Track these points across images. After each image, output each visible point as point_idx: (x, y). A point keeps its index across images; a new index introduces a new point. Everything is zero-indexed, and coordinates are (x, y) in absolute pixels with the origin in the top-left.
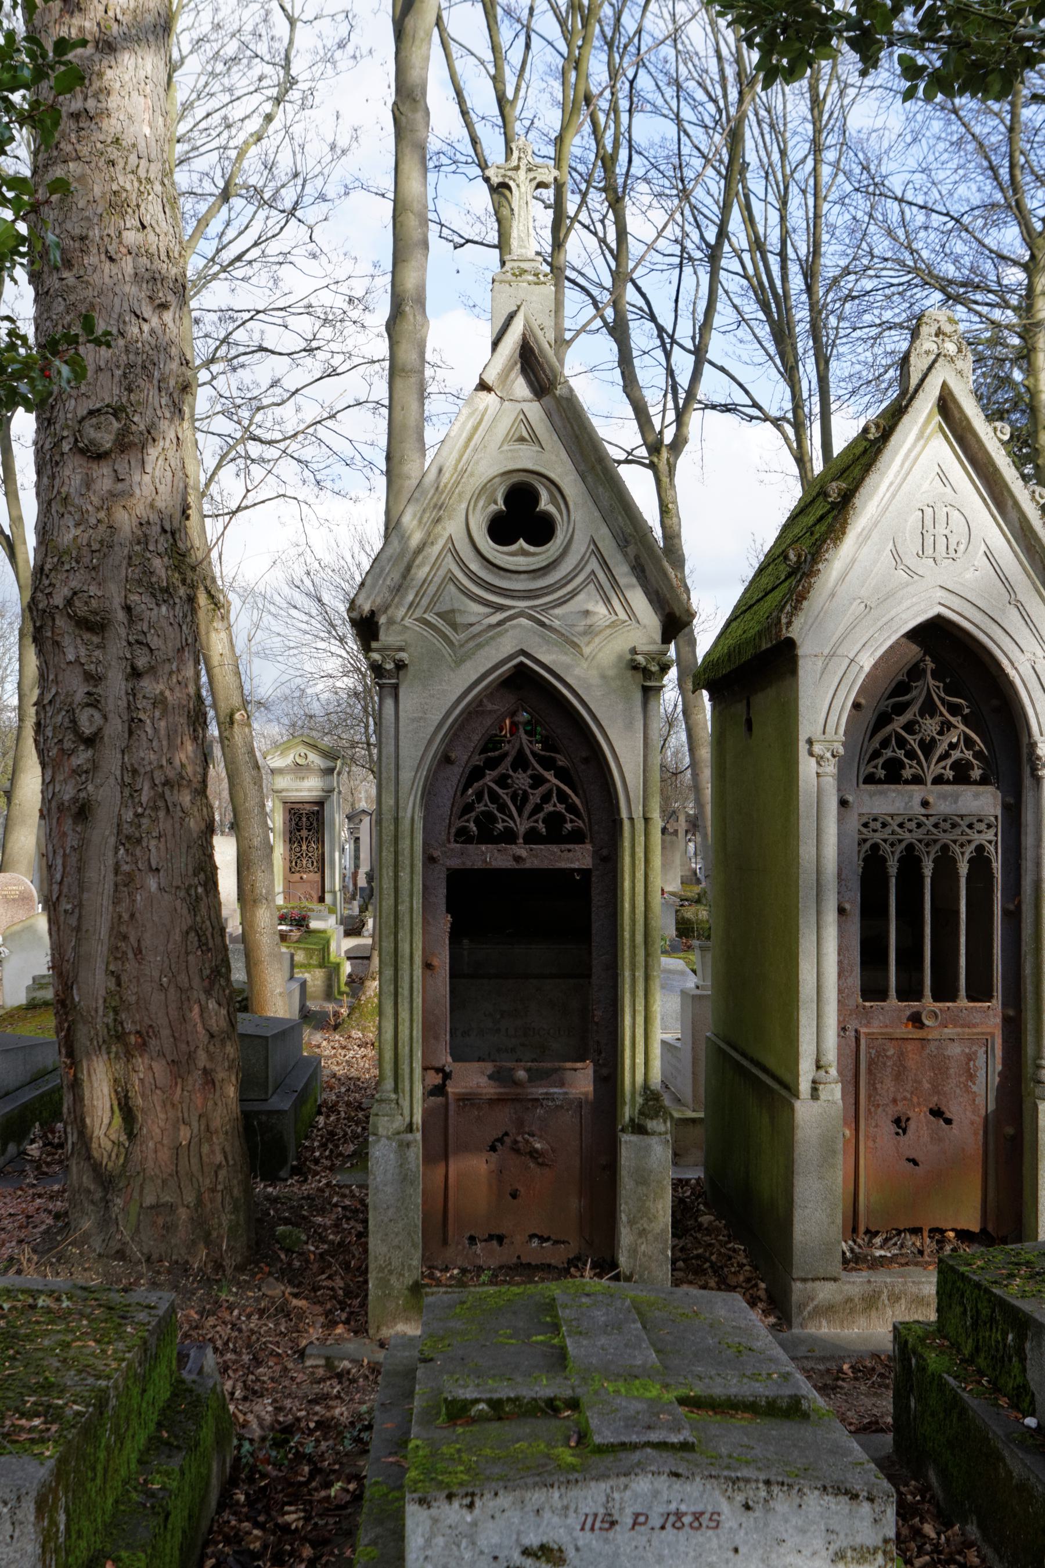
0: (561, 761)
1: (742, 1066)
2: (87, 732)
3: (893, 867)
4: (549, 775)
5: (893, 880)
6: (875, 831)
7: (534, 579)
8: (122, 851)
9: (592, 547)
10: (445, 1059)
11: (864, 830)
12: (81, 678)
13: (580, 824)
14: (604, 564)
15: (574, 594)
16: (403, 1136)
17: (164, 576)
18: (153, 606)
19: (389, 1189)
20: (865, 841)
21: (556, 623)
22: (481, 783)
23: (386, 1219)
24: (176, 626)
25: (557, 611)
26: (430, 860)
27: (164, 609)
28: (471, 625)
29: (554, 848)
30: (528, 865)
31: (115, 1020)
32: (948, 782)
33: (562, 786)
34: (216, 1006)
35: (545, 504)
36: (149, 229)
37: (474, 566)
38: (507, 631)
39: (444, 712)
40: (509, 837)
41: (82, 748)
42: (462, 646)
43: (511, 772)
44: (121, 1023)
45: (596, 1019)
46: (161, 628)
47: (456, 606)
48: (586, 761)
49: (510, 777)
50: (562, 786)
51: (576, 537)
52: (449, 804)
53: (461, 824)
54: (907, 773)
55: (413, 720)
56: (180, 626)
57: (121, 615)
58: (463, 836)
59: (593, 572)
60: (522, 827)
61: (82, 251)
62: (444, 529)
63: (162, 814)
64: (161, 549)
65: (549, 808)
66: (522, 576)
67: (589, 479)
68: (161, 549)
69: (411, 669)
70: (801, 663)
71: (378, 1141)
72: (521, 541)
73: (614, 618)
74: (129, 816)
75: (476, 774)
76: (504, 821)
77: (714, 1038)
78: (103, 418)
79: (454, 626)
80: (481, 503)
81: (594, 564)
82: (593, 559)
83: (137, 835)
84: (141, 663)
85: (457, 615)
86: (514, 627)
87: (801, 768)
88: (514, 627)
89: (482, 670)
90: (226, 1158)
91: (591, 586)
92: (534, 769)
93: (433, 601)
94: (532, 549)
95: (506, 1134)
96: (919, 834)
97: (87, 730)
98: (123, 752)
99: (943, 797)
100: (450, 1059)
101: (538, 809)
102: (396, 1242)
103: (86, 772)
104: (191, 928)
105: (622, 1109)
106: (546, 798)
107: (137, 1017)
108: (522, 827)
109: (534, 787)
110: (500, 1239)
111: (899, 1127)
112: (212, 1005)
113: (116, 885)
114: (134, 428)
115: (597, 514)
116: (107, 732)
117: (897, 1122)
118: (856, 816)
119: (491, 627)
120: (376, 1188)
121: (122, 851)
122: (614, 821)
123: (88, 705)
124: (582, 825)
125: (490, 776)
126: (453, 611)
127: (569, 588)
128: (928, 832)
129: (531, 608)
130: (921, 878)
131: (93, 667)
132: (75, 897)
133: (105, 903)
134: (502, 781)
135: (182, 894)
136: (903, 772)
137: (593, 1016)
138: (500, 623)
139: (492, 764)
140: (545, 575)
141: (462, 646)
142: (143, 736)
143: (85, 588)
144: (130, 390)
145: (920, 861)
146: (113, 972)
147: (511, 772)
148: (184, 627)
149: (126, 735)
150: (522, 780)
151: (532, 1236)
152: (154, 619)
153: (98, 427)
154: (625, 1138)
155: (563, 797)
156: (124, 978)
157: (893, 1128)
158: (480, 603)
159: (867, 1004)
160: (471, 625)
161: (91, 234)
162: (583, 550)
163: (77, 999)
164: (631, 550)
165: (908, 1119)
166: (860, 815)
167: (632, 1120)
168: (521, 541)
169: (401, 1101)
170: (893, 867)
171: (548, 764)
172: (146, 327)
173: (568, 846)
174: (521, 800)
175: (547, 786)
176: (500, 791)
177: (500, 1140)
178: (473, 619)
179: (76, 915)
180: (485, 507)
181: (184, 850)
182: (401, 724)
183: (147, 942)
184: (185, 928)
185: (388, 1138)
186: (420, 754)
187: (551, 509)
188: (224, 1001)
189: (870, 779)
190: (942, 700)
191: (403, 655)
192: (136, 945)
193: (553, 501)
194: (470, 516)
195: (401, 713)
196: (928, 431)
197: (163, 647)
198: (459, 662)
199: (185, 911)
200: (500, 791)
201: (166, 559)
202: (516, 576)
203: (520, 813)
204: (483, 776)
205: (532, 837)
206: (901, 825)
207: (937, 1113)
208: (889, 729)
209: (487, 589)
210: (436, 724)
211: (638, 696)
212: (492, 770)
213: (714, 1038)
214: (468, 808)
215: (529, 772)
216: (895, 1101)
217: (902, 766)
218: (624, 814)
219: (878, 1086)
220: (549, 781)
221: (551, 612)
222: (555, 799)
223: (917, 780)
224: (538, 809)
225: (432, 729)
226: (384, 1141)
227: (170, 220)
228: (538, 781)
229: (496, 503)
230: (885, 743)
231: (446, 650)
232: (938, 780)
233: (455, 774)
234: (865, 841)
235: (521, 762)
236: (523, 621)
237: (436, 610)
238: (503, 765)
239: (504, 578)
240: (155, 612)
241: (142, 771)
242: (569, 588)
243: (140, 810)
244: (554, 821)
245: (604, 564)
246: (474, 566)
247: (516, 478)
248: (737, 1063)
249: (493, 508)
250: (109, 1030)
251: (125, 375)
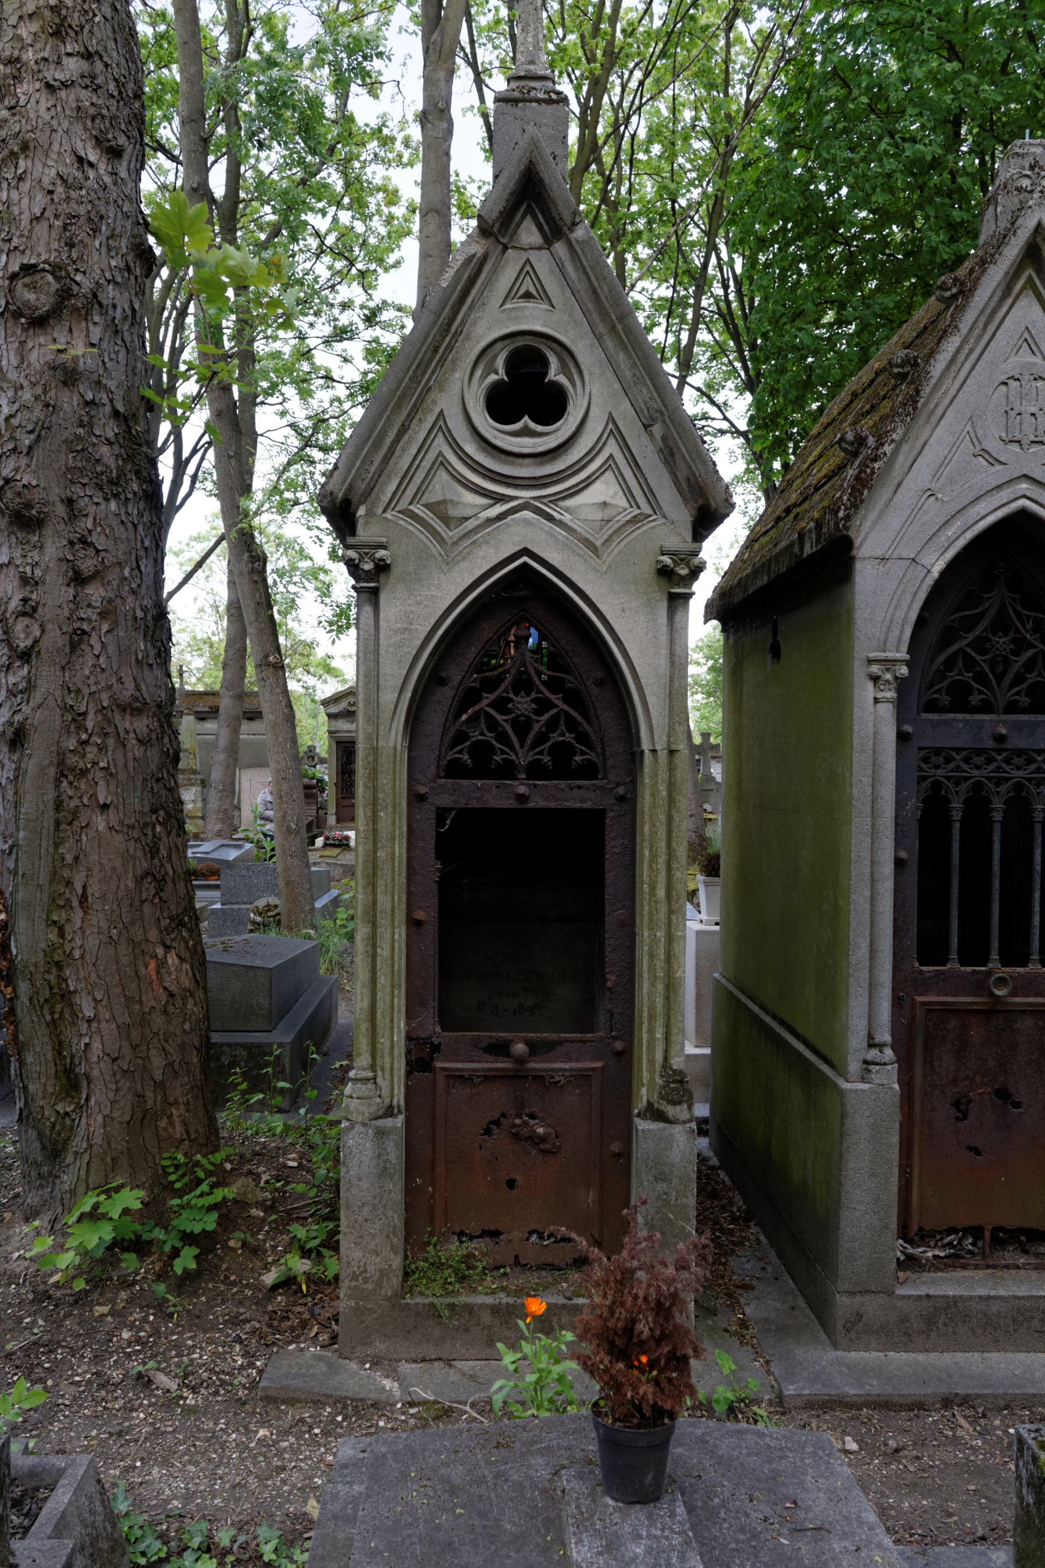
0: (571, 683)
1: (762, 1021)
2: (22, 645)
3: (998, 807)
4: (555, 699)
5: (997, 828)
6: (937, 767)
7: (542, 464)
8: (65, 784)
9: (610, 426)
10: (431, 1027)
11: (925, 766)
12: (16, 582)
13: (592, 756)
14: (624, 446)
15: (588, 483)
16: (380, 1123)
17: (113, 466)
18: (99, 500)
19: (365, 1184)
20: (925, 778)
21: (567, 518)
22: (477, 707)
23: (360, 1219)
24: (129, 526)
25: (569, 503)
26: (416, 799)
27: (113, 505)
28: (466, 519)
29: (563, 784)
30: (531, 805)
31: (59, 976)
32: (1024, 711)
33: (571, 711)
34: (177, 961)
35: (554, 374)
36: (96, 58)
37: (470, 448)
38: (508, 526)
39: (433, 621)
40: (507, 771)
41: (18, 663)
42: (455, 543)
43: (512, 696)
44: (66, 980)
45: (609, 984)
46: (110, 526)
47: (449, 496)
48: (600, 683)
49: (511, 700)
50: (571, 711)
51: (591, 414)
52: (440, 731)
53: (451, 755)
54: (975, 699)
55: (396, 631)
56: (135, 526)
57: (61, 510)
58: (454, 770)
59: (611, 456)
60: (523, 757)
61: (14, 77)
62: (434, 402)
63: (111, 742)
64: (110, 434)
65: (556, 737)
66: (527, 461)
67: (609, 343)
68: (110, 434)
69: (395, 571)
70: (858, 565)
71: (351, 1128)
72: (526, 418)
73: (638, 511)
74: (72, 743)
75: (470, 697)
76: (503, 752)
77: (724, 981)
78: (38, 276)
79: (446, 520)
80: (479, 373)
81: (612, 448)
82: (612, 441)
83: (81, 765)
84: (87, 565)
85: (449, 506)
86: (517, 522)
87: (856, 691)
88: (517, 522)
89: (478, 573)
90: (187, 1131)
91: (609, 475)
92: (539, 691)
93: (419, 492)
94: (539, 428)
95: (504, 1115)
96: (988, 770)
97: (23, 644)
98: (63, 668)
99: (1018, 727)
100: (438, 1029)
101: (542, 738)
102: (372, 1246)
103: (21, 692)
104: (146, 874)
105: (639, 1091)
106: (552, 725)
107: (82, 975)
108: (523, 757)
109: (539, 712)
110: (495, 1234)
111: (959, 1111)
112: (172, 960)
113: (58, 823)
114: (75, 288)
115: (617, 386)
116: (45, 643)
117: (957, 1105)
118: (916, 750)
119: (490, 521)
120: (349, 1182)
121: (65, 784)
122: (633, 754)
123: (24, 614)
124: (595, 759)
125: (488, 698)
126: (444, 502)
127: (583, 475)
128: (999, 769)
129: (535, 498)
130: (949, 822)
131: (28, 569)
132: (11, 836)
133: (44, 844)
134: (501, 706)
135: (136, 834)
136: (971, 698)
137: (605, 981)
138: (500, 517)
139: (490, 685)
140: (555, 459)
141: (455, 543)
142: (87, 649)
143: (18, 477)
144: (71, 245)
145: (949, 802)
146: (55, 922)
147: (512, 696)
148: (140, 528)
149: (67, 650)
150: (523, 704)
151: (531, 1233)
152: (101, 515)
153: (32, 287)
154: (642, 1125)
155: (572, 725)
156: (68, 929)
157: (953, 1112)
158: (476, 492)
159: (925, 968)
160: (466, 519)
161: (24, 57)
162: (600, 429)
163: (14, 952)
164: (657, 430)
165: (970, 1101)
166: (920, 749)
167: (650, 1105)
168: (526, 418)
169: (379, 1080)
170: (998, 807)
171: (554, 685)
172: (92, 174)
173: (577, 782)
174: (522, 727)
175: (554, 711)
176: (500, 718)
177: (497, 1123)
178: (468, 512)
179: (14, 857)
180: (484, 377)
181: (139, 784)
182: (382, 636)
183: (94, 889)
184: (139, 872)
185: (364, 1125)
186: (404, 672)
187: (562, 379)
188: (186, 955)
189: (932, 706)
190: (1019, 615)
191: (381, 553)
192: (80, 892)
193: (564, 369)
194: (466, 396)
195: (382, 623)
196: (1018, 287)
197: (112, 549)
198: (450, 563)
199: (140, 854)
200: (500, 718)
201: (116, 447)
202: (520, 460)
203: (522, 745)
204: (479, 699)
205: (536, 771)
206: (967, 761)
207: (1003, 1094)
208: (955, 647)
209: (485, 477)
210: (423, 636)
211: (664, 604)
212: (491, 692)
213: (724, 981)
214: (461, 737)
215: (533, 695)
216: (954, 1081)
217: (969, 690)
218: (646, 746)
219: (936, 1063)
220: (557, 706)
221: (562, 504)
222: (563, 727)
223: (986, 708)
224: (542, 738)
225: (419, 642)
226: (358, 1128)
227: (122, 51)
228: (543, 705)
229: (497, 373)
230: (950, 664)
231: (436, 548)
232: (1012, 708)
233: (446, 696)
234: (925, 778)
235: (523, 685)
236: (527, 514)
237: (424, 500)
238: (502, 687)
239: (506, 463)
240: (103, 507)
241: (86, 691)
242: (583, 475)
243: (84, 736)
244: (562, 752)
245: (624, 446)
246: (470, 448)
247: (520, 342)
248: (756, 1017)
249: (493, 377)
250: (51, 988)
251: (65, 227)
